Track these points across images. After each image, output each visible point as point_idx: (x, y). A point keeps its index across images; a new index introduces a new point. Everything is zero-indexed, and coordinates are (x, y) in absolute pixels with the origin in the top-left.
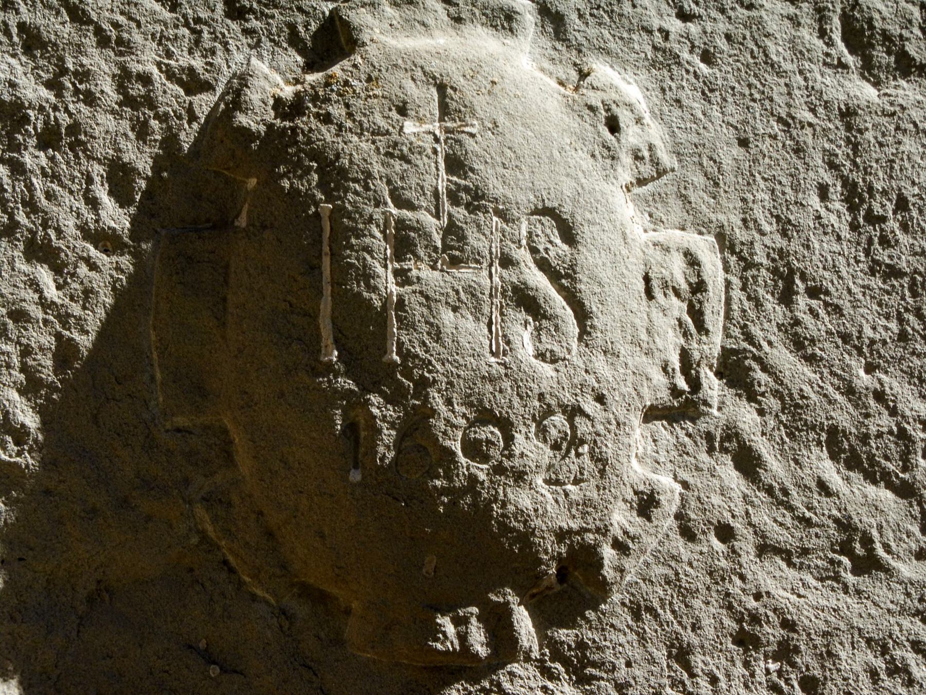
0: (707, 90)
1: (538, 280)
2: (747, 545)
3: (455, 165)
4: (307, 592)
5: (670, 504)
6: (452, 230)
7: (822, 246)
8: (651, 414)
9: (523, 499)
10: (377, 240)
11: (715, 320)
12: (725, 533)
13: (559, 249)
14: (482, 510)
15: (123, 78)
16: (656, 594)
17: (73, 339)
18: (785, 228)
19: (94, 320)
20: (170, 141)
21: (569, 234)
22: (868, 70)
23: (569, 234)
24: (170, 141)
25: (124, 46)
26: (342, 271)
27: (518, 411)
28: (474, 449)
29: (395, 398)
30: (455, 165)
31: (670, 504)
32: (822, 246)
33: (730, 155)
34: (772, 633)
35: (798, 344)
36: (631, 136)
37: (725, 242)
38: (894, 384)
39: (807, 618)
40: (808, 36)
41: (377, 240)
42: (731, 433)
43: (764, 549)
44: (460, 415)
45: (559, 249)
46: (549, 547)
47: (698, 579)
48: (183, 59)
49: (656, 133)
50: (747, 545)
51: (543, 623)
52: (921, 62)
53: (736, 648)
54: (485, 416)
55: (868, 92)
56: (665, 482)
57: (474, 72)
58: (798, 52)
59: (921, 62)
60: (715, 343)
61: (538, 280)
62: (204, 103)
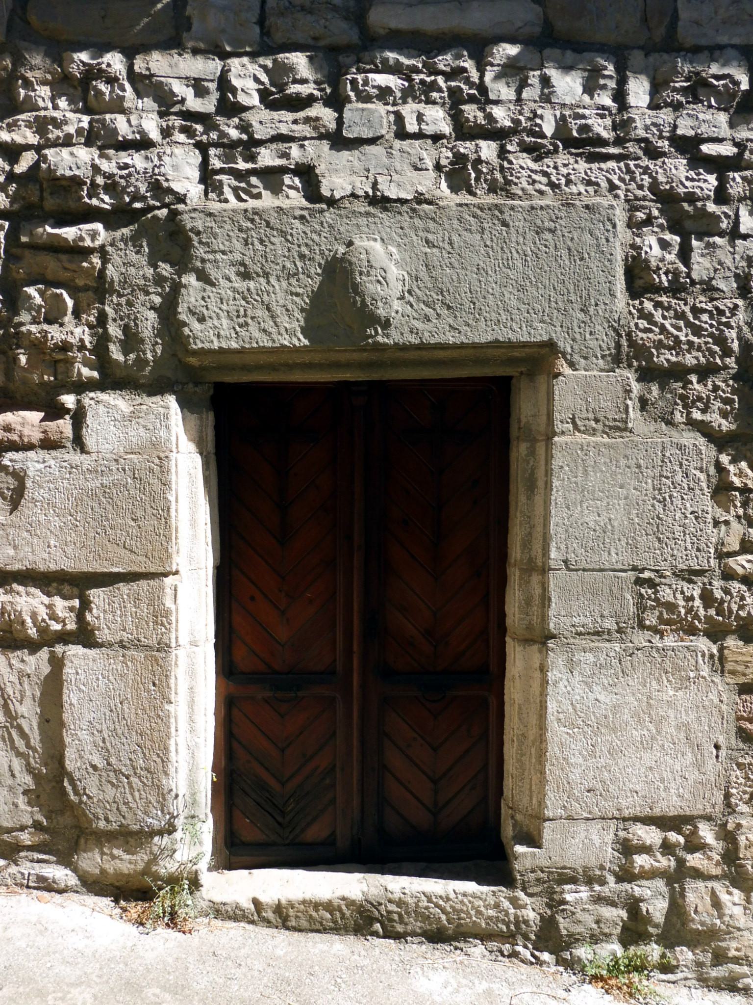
0: (405, 250)
1: (381, 279)
2: (411, 318)
3: (368, 262)
4: (348, 326)
5: (400, 312)
6: (368, 271)
7: (422, 273)
8: (398, 299)
9: (379, 312)
10: (357, 273)
11: (407, 285)
12: (408, 316)
13: (383, 274)
14: (373, 313)
15: (320, 250)
16: (398, 325)
17: (75, 175)
18: (417, 271)
19: (317, 286)
20: (327, 259)
21: (385, 272)
22: (429, 247)
23: (385, 272)
24: (327, 259)
25: (320, 245)
26: (352, 278)
27: (378, 299)
28: (372, 304)
29: (360, 297)
30: (368, 262)
31: (400, 312)
32: (422, 273)
33: (409, 260)
34: (415, 331)
35: (419, 288)
36: (394, 257)
37: (408, 273)
38: (432, 294)
39: (420, 329)
40: (420, 242)
41: (357, 273)
42: (409, 301)
43: (414, 318)
44: (370, 299)
45: (383, 274)
46: (383, 319)
47: (404, 323)
48: (328, 247)
49: (398, 257)
50: (411, 318)
51: (382, 330)
52: (475, 122)
53: (29, 809)
54: (373, 299)
55: (428, 250)
56: (400, 309)
57: (371, 247)
58: (418, 244)
59: (475, 122)
60: (407, 288)
61: (381, 279)
62: (332, 254)
